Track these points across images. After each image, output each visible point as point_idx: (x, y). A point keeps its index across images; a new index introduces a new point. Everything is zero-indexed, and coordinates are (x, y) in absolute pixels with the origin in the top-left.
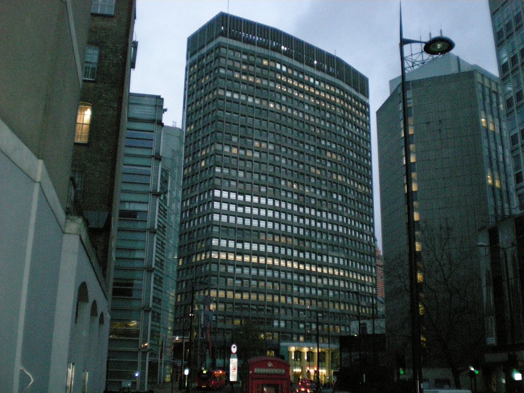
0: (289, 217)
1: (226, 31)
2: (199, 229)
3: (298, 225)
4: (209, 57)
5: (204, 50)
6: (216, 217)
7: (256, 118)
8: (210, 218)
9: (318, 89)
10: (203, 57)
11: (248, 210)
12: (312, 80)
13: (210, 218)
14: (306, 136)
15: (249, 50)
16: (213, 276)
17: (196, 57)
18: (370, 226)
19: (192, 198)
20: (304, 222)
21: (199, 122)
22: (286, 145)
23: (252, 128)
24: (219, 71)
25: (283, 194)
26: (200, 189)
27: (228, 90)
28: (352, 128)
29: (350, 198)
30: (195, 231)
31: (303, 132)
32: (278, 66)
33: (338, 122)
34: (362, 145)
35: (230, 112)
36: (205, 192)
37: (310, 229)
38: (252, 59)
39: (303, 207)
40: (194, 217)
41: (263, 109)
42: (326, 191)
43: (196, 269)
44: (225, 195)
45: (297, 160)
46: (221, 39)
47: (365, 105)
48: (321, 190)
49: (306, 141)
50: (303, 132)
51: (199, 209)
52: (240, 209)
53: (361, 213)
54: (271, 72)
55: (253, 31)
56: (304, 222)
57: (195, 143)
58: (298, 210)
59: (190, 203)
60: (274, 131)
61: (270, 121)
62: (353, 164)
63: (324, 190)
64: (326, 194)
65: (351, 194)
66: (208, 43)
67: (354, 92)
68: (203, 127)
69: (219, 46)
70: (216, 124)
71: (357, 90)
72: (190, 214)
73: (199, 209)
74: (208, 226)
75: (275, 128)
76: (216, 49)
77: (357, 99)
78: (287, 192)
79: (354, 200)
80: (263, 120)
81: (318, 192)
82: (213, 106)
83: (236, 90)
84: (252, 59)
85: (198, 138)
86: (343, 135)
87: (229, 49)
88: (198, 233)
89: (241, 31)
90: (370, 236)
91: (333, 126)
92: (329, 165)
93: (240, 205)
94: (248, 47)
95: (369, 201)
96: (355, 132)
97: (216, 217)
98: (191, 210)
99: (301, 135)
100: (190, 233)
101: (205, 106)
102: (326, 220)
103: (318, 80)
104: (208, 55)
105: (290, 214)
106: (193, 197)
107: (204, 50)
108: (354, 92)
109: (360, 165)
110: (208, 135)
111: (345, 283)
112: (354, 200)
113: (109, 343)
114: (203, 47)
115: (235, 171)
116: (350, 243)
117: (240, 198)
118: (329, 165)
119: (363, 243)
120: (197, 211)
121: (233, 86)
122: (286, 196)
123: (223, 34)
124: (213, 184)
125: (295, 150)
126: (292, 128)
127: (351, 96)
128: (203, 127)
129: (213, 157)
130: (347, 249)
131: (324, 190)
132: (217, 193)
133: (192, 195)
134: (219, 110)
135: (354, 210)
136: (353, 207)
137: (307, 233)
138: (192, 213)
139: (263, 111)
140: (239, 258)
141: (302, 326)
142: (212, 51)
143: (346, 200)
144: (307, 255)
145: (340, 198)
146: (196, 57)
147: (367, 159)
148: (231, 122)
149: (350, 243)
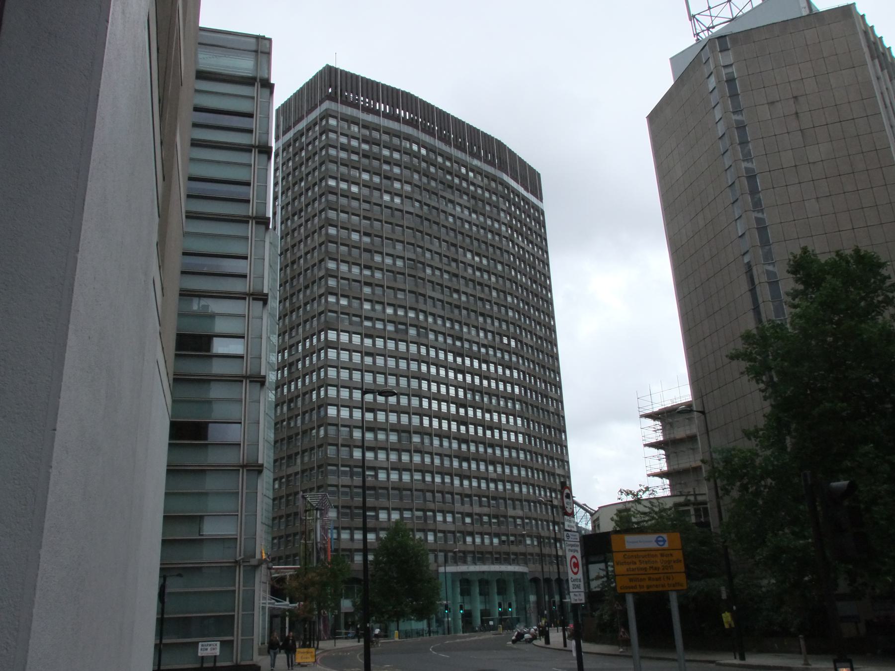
0: (444, 406)
1: (336, 93)
2: (304, 394)
3: (455, 383)
4: (310, 133)
5: (302, 125)
6: (332, 411)
7: (386, 222)
8: (322, 374)
9: (473, 184)
10: (302, 135)
11: (380, 361)
12: (463, 170)
13: (322, 374)
14: (460, 250)
15: (371, 122)
16: (330, 465)
17: (290, 135)
18: (555, 386)
19: (291, 347)
20: (464, 378)
21: (298, 297)
22: (431, 247)
23: (381, 237)
24: (327, 122)
25: (431, 336)
26: (304, 330)
27: (343, 296)
28: (523, 242)
29: (526, 344)
30: (298, 396)
31: (455, 245)
32: (415, 147)
33: (502, 206)
34: (538, 268)
35: (347, 213)
36: (312, 372)
37: (473, 389)
38: (376, 135)
39: (462, 356)
40: (295, 375)
41: (397, 210)
42: (492, 332)
43: (302, 477)
44: (344, 337)
45: (449, 285)
46: (327, 105)
47: (538, 211)
48: (486, 331)
49: (463, 288)
50: (455, 245)
51: (304, 345)
52: (368, 360)
53: (543, 367)
54: (404, 156)
55: (375, 97)
56: (464, 378)
57: (293, 263)
58: (455, 360)
59: (290, 355)
60: (413, 242)
61: (407, 227)
62: (528, 294)
63: (490, 331)
64: (494, 337)
65: (527, 339)
66: (310, 111)
67: (521, 190)
68: (306, 238)
69: (326, 115)
70: (327, 247)
71: (526, 189)
72: (290, 372)
73: (304, 345)
74: (319, 407)
75: (414, 237)
76: (321, 120)
77: (526, 201)
78: (436, 333)
79: (532, 347)
80: (397, 225)
81: (482, 334)
82: (319, 287)
83: (354, 212)
84: (376, 135)
85: (298, 255)
86: (512, 251)
87: (342, 119)
88: (303, 400)
89: (358, 95)
90: (556, 400)
91: (497, 238)
92: (494, 294)
93: (368, 354)
94: (370, 118)
95: (552, 349)
96: (526, 248)
97: (332, 373)
98: (291, 365)
99: (453, 249)
100: (291, 401)
101: (307, 206)
102: (495, 376)
103: (472, 171)
104: (308, 130)
105: (442, 367)
106: (293, 345)
107: (302, 125)
108: (521, 190)
109: (537, 296)
110: (314, 248)
111: (521, 405)
112: (532, 347)
113: (169, 450)
114: (301, 119)
115: (358, 301)
116: (530, 411)
117: (368, 342)
118: (494, 294)
119: (548, 412)
120: (300, 366)
121: (349, 205)
122: (436, 339)
123: (332, 98)
124: (327, 252)
125: (445, 271)
126: (439, 239)
127: (518, 196)
128: (306, 238)
129: (323, 247)
130: (536, 520)
131: (490, 331)
132: (332, 335)
133: (293, 341)
134: (331, 209)
135: (533, 362)
136: (531, 358)
137: (469, 396)
138: (293, 370)
139: (396, 213)
140: (369, 416)
141: (468, 520)
142: (315, 124)
143: (522, 346)
144: (471, 412)
145: (513, 343)
146: (290, 135)
147: (546, 288)
148: (349, 227)
149: (530, 411)
